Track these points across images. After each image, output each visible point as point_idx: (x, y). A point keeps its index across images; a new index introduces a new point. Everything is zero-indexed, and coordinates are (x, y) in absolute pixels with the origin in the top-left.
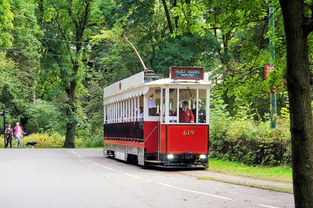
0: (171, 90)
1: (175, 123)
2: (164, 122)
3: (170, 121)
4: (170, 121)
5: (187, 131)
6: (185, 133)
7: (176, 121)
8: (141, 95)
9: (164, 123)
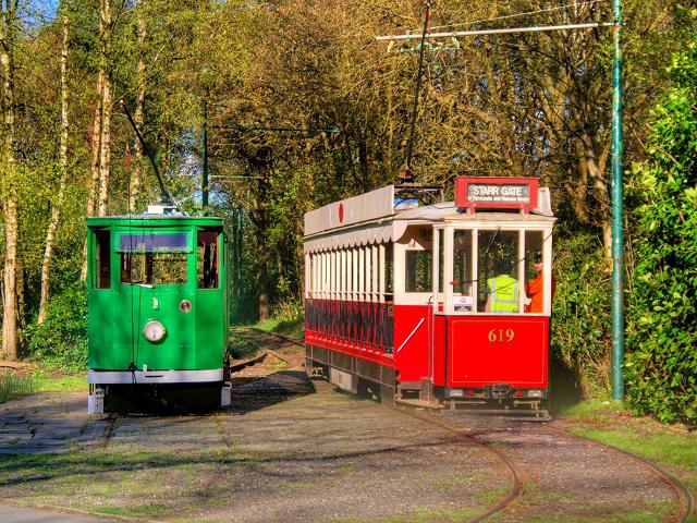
0: (458, 233)
1: (467, 313)
2: (441, 309)
3: (456, 308)
4: (456, 308)
5: (497, 333)
6: (491, 336)
7: (469, 308)
8: (386, 241)
9: (440, 313)
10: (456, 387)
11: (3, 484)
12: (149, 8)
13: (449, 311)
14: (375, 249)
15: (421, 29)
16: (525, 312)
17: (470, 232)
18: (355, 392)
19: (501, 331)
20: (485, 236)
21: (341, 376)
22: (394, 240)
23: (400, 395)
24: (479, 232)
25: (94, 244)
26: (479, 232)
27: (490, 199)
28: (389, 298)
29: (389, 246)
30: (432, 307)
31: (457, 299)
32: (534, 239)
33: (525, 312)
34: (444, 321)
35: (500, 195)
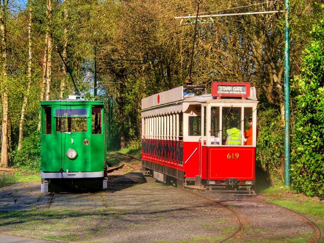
0: (213, 108)
1: (217, 146)
2: (205, 143)
3: (212, 143)
4: (212, 143)
5: (231, 155)
6: (228, 156)
7: (218, 143)
8: (180, 112)
9: (205, 145)
10: (212, 180)
11: (1, 225)
12: (69, 4)
13: (209, 145)
14: (174, 116)
15: (196, 13)
16: (244, 145)
17: (218, 108)
18: (165, 182)
19: (233, 154)
20: (225, 110)
21: (158, 175)
22: (183, 111)
23: (186, 183)
24: (223, 108)
25: (44, 113)
26: (223, 108)
27: (228, 92)
28: (181, 138)
29: (181, 114)
30: (201, 143)
31: (213, 139)
32: (248, 111)
33: (244, 145)
34: (206, 149)
35: (233, 91)
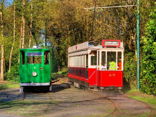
0: (103, 52)
1: (105, 70)
2: (99, 69)
3: (102, 69)
4: (102, 69)
5: (111, 75)
6: (110, 75)
7: (105, 69)
8: (86, 54)
9: (99, 70)
10: (102, 87)
11: (1, 108)
12: (33, 2)
13: (100, 70)
14: (84, 56)
15: (94, 6)
16: (118, 70)
17: (105, 52)
18: (80, 88)
19: (112, 74)
20: (108, 53)
21: (76, 84)
22: (88, 54)
23: (90, 88)
24: (107, 52)
25: (21, 55)
26: (107, 52)
27: (110, 44)
28: (87, 67)
29: (87, 55)
30: (97, 69)
31: (102, 67)
32: (120, 53)
33: (118, 70)
34: (99, 72)
35: (112, 44)
